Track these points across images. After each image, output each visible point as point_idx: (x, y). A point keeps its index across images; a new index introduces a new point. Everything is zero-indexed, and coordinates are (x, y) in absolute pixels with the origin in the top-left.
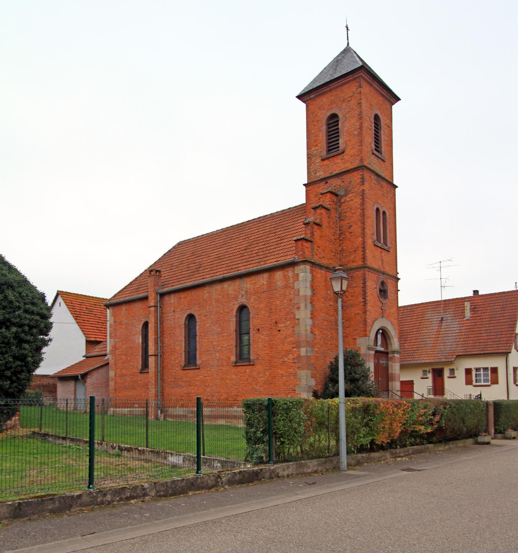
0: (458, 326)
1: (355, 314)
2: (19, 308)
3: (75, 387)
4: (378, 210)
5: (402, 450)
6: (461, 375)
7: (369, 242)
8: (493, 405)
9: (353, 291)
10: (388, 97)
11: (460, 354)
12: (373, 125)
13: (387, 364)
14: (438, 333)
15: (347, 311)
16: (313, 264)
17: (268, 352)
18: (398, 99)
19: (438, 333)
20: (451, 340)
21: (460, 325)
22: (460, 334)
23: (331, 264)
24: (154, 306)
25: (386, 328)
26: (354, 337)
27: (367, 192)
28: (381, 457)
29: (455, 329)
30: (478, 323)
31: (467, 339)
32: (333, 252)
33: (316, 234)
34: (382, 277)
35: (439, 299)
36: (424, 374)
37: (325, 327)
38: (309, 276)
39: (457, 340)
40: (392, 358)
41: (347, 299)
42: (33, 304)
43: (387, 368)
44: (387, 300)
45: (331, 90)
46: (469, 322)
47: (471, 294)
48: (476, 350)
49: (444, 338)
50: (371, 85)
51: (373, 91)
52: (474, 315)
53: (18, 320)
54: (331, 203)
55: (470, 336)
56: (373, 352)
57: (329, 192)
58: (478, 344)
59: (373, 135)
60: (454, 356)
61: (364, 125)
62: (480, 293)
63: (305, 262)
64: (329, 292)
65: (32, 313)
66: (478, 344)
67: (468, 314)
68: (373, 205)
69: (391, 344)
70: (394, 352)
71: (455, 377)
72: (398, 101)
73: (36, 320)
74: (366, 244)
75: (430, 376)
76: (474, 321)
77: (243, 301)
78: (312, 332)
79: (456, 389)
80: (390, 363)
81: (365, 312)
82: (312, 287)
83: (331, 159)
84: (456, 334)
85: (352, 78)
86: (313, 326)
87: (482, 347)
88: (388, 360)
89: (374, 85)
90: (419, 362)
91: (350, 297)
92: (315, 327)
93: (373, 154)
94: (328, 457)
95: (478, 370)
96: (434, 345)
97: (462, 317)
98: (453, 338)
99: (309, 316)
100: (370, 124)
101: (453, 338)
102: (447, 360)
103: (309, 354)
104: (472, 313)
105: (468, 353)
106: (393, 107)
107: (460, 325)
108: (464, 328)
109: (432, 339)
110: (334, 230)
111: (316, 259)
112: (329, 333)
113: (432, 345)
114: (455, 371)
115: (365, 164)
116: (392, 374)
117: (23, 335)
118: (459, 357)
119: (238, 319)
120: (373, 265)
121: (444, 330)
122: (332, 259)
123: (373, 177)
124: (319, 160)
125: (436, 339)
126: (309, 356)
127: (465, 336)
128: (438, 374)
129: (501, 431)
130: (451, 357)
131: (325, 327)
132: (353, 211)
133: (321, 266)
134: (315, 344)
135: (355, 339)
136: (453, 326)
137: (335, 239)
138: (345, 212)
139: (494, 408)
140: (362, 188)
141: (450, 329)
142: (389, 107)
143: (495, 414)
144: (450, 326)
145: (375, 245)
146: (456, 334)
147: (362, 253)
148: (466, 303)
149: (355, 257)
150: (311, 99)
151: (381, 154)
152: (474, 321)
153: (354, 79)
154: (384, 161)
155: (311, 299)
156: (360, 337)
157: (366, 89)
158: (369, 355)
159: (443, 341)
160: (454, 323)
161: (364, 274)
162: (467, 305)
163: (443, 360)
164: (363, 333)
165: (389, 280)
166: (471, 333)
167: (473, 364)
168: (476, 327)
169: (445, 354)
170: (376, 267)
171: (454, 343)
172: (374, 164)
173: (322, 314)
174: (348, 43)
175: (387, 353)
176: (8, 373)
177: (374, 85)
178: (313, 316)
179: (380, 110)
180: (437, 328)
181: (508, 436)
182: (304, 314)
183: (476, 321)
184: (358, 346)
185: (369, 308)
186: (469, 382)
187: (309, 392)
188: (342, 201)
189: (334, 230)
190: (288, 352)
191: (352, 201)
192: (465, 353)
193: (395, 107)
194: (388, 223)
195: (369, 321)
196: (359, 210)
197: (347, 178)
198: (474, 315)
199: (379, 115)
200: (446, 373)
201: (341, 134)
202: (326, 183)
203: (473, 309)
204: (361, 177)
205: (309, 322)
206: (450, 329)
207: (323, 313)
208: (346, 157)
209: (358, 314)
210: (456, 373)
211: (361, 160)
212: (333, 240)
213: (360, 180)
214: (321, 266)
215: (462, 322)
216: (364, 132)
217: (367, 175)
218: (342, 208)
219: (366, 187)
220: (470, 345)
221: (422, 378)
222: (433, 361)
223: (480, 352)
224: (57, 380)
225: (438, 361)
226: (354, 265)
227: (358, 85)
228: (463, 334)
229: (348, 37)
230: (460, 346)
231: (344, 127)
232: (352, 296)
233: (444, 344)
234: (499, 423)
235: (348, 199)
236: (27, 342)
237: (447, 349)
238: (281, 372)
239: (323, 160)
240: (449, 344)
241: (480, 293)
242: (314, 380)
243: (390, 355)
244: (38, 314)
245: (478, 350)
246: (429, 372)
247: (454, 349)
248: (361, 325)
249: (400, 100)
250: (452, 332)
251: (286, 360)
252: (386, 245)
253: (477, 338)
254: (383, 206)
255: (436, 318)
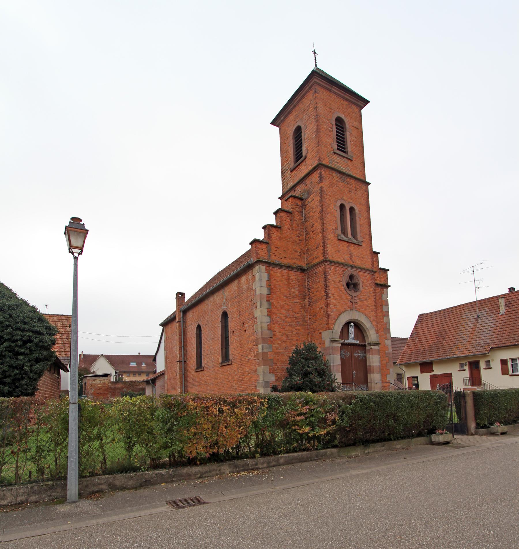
0: (493, 321)
1: (320, 309)
2: (8, 326)
3: (152, 389)
4: (342, 207)
5: (262, 460)
6: (496, 365)
7: (331, 237)
8: (471, 395)
9: (317, 287)
10: (355, 101)
11: (494, 346)
12: (334, 127)
13: (365, 357)
14: (473, 329)
15: (314, 307)
16: (268, 264)
17: (239, 351)
18: (366, 102)
19: (473, 329)
20: (486, 335)
21: (495, 321)
22: (496, 328)
23: (295, 263)
24: (179, 322)
25: (357, 320)
26: (320, 331)
27: (326, 189)
28: (205, 472)
29: (490, 324)
30: (513, 317)
31: (502, 332)
32: (297, 252)
33: (274, 236)
34: (350, 271)
35: (473, 299)
36: (461, 367)
37: (288, 324)
38: (265, 276)
39: (491, 334)
40: (369, 350)
41: (313, 295)
42: (25, 323)
43: (364, 360)
44: (358, 293)
45: (295, 106)
46: (504, 316)
47: (507, 291)
48: (510, 341)
49: (479, 333)
50: (330, 91)
51: (333, 96)
52: (509, 310)
53: (9, 336)
54: (295, 207)
55: (505, 329)
56: (340, 345)
57: (291, 196)
58: (512, 336)
59: (335, 137)
60: (489, 349)
61: (321, 127)
62: (516, 290)
63: (259, 262)
64: (293, 290)
65: (23, 330)
66: (512, 336)
67: (503, 309)
68: (336, 201)
69: (368, 336)
70: (370, 344)
71: (491, 368)
72: (367, 104)
73: (28, 336)
74: (326, 239)
75: (467, 368)
76: (509, 315)
77: (224, 307)
78: (269, 329)
79: (493, 380)
80: (368, 356)
81: (327, 306)
82: (270, 285)
83: (297, 168)
84: (491, 329)
85: (308, 87)
86: (272, 322)
87: (516, 338)
88: (365, 353)
89: (333, 89)
90: (454, 356)
91: (315, 293)
92: (274, 324)
93: (335, 153)
94: (460, 429)
95: (513, 360)
96: (470, 340)
97: (497, 313)
98: (488, 332)
99: (266, 314)
100: (331, 126)
101: (488, 332)
102: (481, 353)
103: (265, 351)
104: (507, 308)
105: (502, 345)
106: (363, 111)
107: (495, 321)
108: (499, 322)
109: (468, 335)
110: (298, 232)
111: (274, 259)
112: (294, 330)
113: (468, 340)
114: (491, 363)
115: (324, 162)
116: (370, 366)
117: (17, 349)
118: (492, 349)
119: (224, 325)
120: (337, 259)
121: (479, 326)
122: (296, 258)
123: (334, 174)
124: (289, 173)
125: (472, 335)
126: (267, 353)
127: (499, 330)
128: (474, 366)
129: (485, 425)
130: (485, 350)
131: (288, 324)
132: (314, 210)
133: (280, 266)
134: (275, 340)
135: (321, 333)
136: (488, 322)
137: (300, 240)
138: (308, 213)
139: (474, 399)
140: (320, 185)
141: (485, 325)
142: (357, 110)
143: (475, 405)
144: (485, 323)
145: (339, 240)
146: (491, 329)
147: (322, 248)
148: (500, 300)
149: (317, 254)
150: (282, 121)
151: (347, 154)
152: (509, 315)
153: (310, 88)
154: (352, 160)
155: (268, 297)
156: (324, 331)
157: (323, 94)
158: (333, 348)
159: (478, 336)
160: (489, 319)
161: (325, 268)
162: (502, 302)
163: (477, 353)
164: (326, 326)
165: (360, 273)
166: (505, 326)
167: (508, 355)
168: (511, 320)
169: (479, 348)
170: (342, 261)
171: (488, 337)
172: (337, 163)
173: (284, 312)
174: (316, 65)
175: (364, 346)
176: (8, 380)
177: (333, 89)
178: (270, 314)
179: (343, 113)
180: (472, 325)
181: (495, 431)
182: (260, 313)
183: (511, 315)
184: (323, 340)
185: (332, 300)
186: (505, 372)
187: (267, 387)
188: (306, 203)
189: (298, 232)
190: (251, 350)
191: (314, 201)
192: (499, 346)
193: (365, 111)
194: (358, 219)
195: (332, 314)
196: (319, 207)
197: (308, 181)
198: (509, 310)
199: (343, 117)
200: (482, 365)
201: (303, 141)
202: (295, 191)
203: (508, 305)
204: (318, 175)
205: (267, 319)
206: (485, 325)
207: (285, 310)
208: (308, 161)
209: (322, 308)
210: (492, 365)
211: (319, 160)
212: (298, 241)
213: (318, 179)
214: (280, 266)
215: (497, 318)
216: (322, 133)
217: (325, 173)
218: (306, 210)
219: (325, 184)
220: (505, 337)
221: (460, 371)
222: (467, 354)
223: (514, 344)
224: (145, 384)
225: (472, 354)
226: (317, 261)
227: (313, 92)
228: (498, 328)
229: (316, 60)
230: (495, 339)
231: (306, 135)
232: (317, 292)
233: (479, 339)
234: (481, 416)
235: (310, 200)
236: (22, 354)
237: (481, 343)
238: (247, 370)
239: (292, 171)
240: (484, 338)
241: (516, 290)
242: (274, 375)
243: (367, 348)
244: (30, 330)
245: (512, 341)
246: (466, 365)
247: (488, 342)
248: (325, 319)
249: (369, 102)
250: (487, 327)
251: (250, 357)
252: (357, 240)
253: (512, 331)
254: (349, 202)
255: (472, 317)
